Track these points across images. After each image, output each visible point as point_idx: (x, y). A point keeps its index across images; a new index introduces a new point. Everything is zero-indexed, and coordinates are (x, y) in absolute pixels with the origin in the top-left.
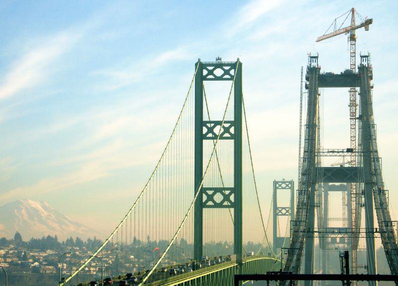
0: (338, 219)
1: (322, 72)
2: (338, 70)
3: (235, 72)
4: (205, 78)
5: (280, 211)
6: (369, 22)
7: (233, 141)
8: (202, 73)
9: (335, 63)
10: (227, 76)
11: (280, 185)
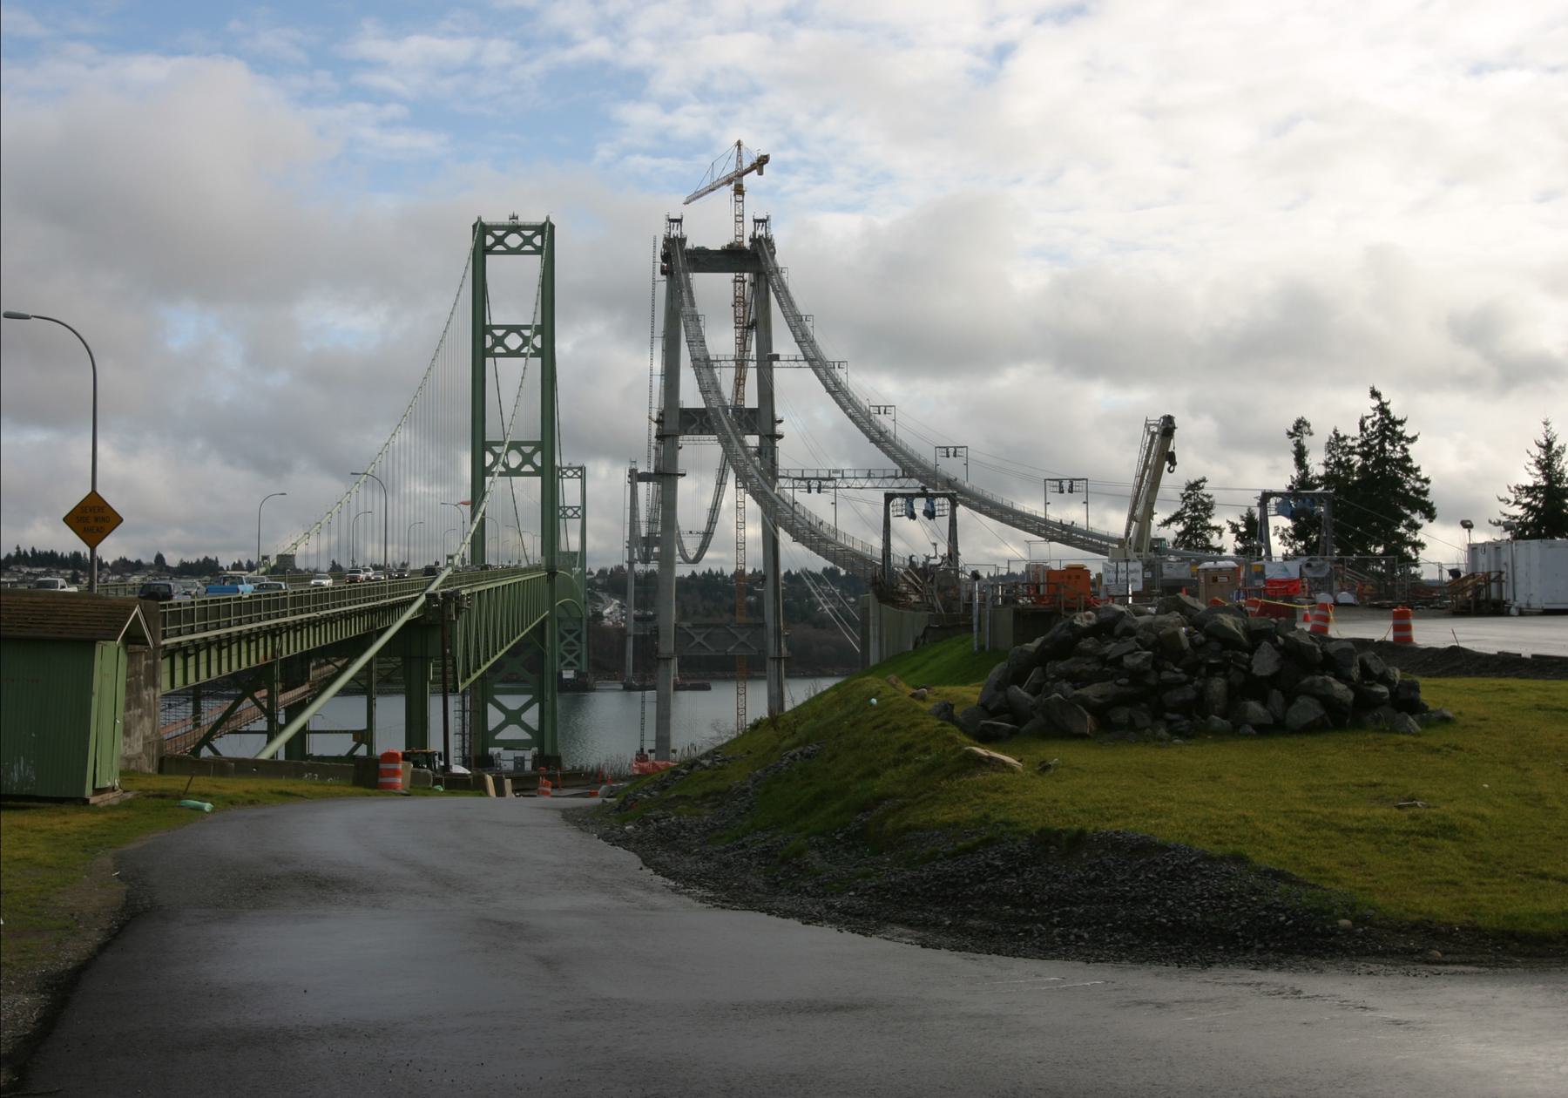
1: (689, 245)
4: (488, 250)
6: (762, 161)
7: (539, 479)
8: (486, 241)
9: (712, 228)
10: (528, 248)
11: (500, 240)
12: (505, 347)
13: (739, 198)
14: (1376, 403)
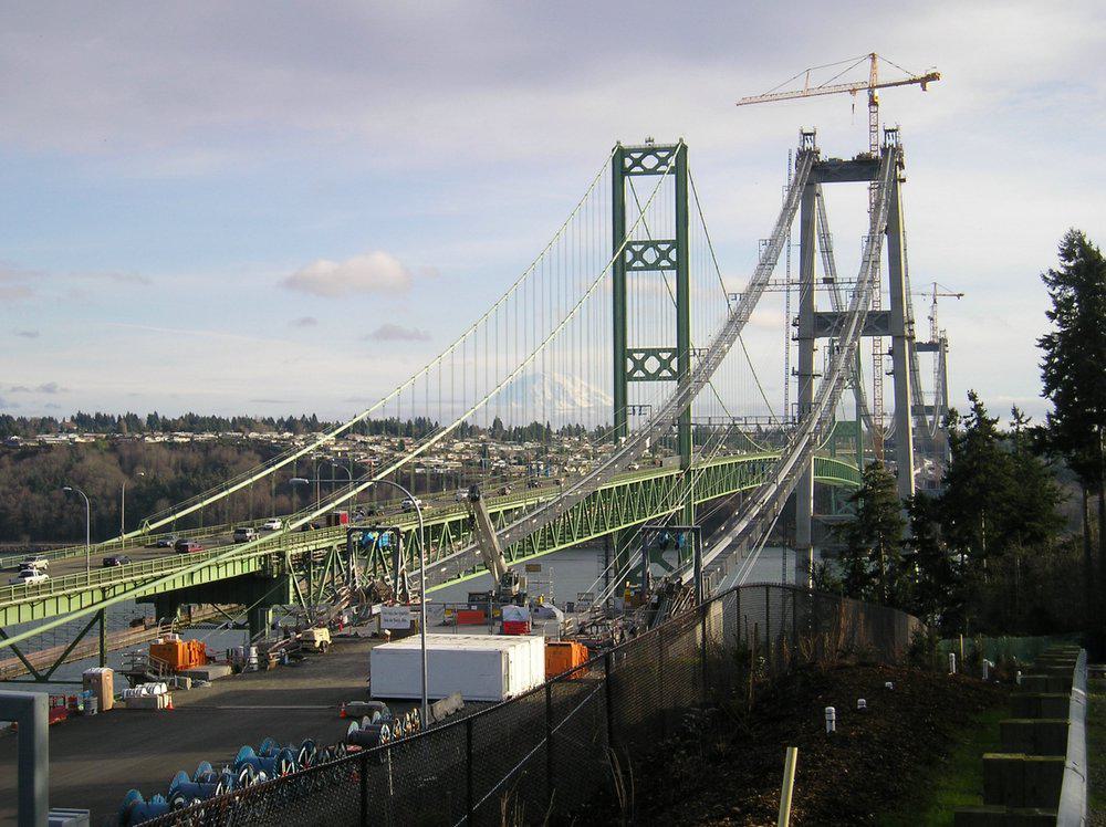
2: (847, 155)
3: (677, 161)
8: (623, 165)
13: (874, 108)
14: (972, 404)
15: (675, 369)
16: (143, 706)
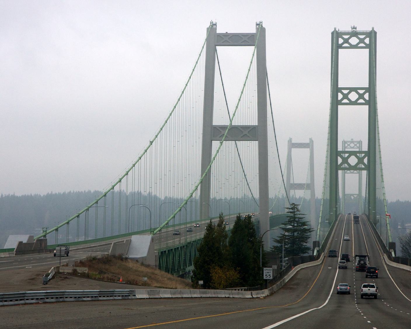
0: (216, 218)
3: (370, 41)
4: (340, 46)
5: (361, 96)
7: (367, 106)
8: (338, 41)
11: (349, 145)
12: (349, 99)
15: (367, 98)
16: (233, 127)
